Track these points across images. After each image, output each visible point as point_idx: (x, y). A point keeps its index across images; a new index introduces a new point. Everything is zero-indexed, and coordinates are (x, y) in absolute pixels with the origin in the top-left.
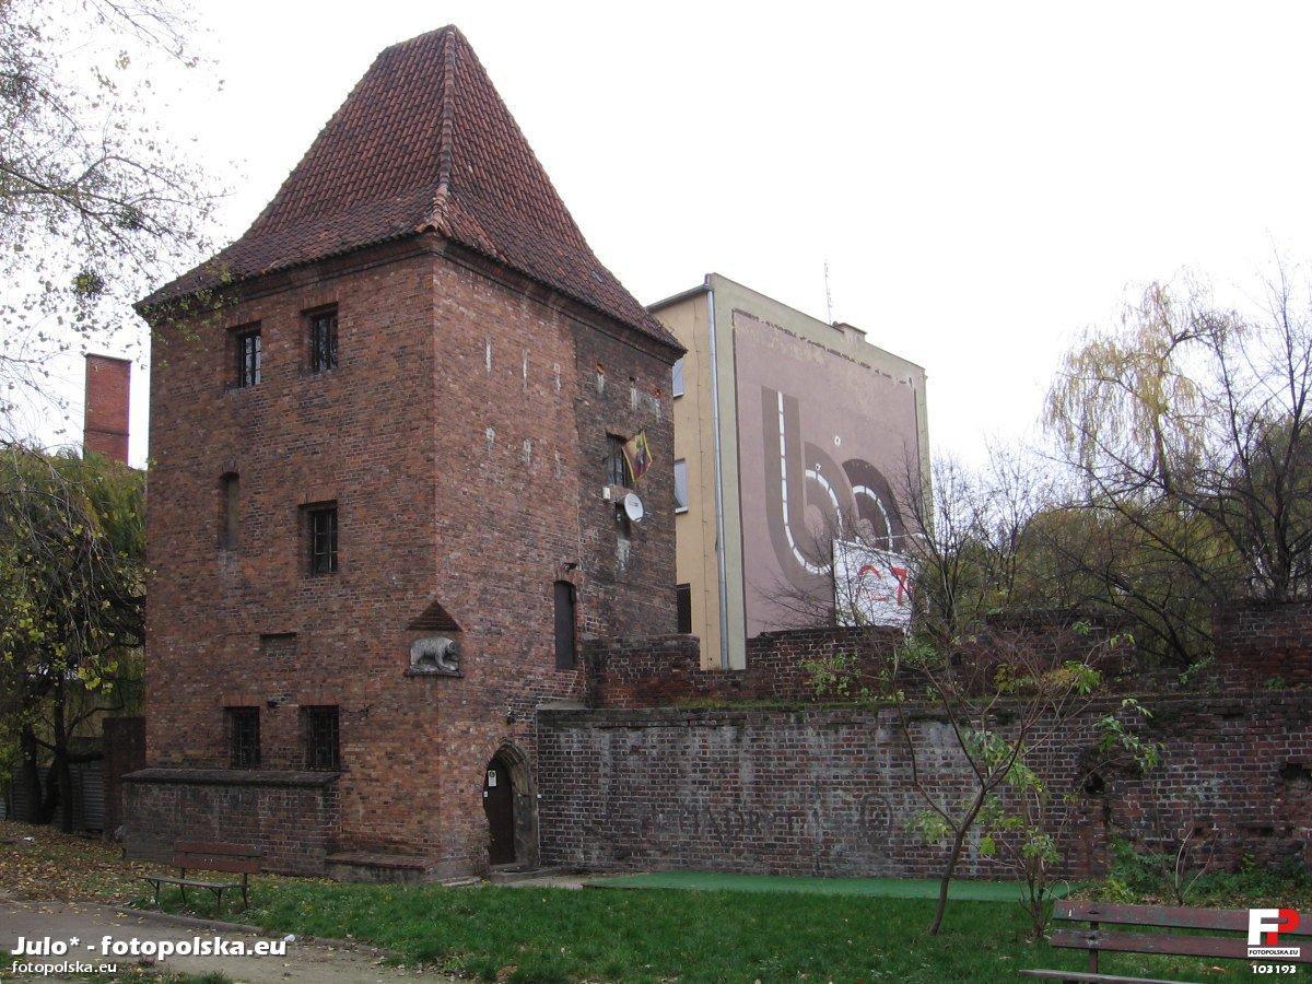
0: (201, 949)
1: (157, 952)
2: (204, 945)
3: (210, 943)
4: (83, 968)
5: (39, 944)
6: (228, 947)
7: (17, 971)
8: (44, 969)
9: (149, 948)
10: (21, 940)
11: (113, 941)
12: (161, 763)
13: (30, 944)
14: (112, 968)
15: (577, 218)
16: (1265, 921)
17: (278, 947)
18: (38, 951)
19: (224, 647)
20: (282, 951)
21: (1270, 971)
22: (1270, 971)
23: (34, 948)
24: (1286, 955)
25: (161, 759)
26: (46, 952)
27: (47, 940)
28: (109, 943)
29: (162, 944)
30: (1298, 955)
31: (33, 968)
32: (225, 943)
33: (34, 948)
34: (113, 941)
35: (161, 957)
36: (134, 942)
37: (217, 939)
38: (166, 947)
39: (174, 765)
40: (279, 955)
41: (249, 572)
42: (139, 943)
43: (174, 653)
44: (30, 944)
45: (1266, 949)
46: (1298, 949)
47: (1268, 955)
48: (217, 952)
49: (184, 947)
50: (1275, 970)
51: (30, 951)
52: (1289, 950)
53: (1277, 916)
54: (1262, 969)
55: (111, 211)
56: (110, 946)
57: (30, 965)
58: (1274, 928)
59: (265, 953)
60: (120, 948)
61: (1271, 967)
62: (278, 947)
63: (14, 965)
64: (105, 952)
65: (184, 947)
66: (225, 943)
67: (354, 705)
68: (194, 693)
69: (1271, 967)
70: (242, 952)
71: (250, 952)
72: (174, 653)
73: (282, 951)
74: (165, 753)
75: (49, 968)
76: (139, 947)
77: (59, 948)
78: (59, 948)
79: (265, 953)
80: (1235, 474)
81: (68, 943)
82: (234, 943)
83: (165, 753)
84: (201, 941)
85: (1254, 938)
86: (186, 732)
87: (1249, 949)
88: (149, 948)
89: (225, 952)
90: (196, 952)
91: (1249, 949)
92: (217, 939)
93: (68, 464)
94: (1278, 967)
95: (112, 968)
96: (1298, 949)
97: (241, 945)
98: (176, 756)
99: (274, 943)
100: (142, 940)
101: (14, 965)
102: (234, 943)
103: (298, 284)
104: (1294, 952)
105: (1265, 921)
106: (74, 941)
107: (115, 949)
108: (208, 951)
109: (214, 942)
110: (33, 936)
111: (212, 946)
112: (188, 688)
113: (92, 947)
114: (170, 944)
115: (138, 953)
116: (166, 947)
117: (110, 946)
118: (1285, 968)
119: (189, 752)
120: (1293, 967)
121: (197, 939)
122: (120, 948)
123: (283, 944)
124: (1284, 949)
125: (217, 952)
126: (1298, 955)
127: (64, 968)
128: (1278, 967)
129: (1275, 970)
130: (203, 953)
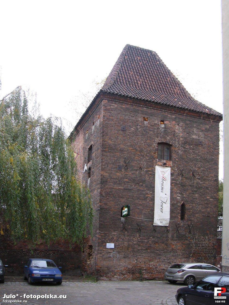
0: (47, 297)
1: (37, 297)
2: (48, 296)
3: (49, 295)
4: (19, 301)
5: (9, 296)
6: (53, 296)
7: (45, 295)
8: (10, 302)
9: (35, 297)
10: (5, 295)
11: (26, 295)
13: (7, 296)
14: (26, 301)
16: (218, 290)
18: (9, 297)
20: (66, 297)
21: (219, 302)
22: (219, 302)
23: (8, 297)
24: (223, 298)
26: (11, 298)
27: (11, 295)
28: (25, 295)
29: (38, 296)
30: (226, 298)
31: (8, 301)
33: (8, 297)
34: (26, 295)
35: (37, 299)
36: (31, 295)
37: (51, 295)
38: (39, 297)
40: (65, 298)
42: (32, 295)
45: (218, 297)
46: (226, 297)
47: (219, 298)
48: (50, 298)
49: (43, 297)
50: (220, 302)
51: (7, 297)
52: (224, 297)
53: (221, 289)
54: (217, 302)
55: (42, 182)
57: (7, 301)
58: (220, 292)
59: (62, 298)
60: (28, 297)
61: (219, 301)
63: (3, 301)
64: (24, 298)
65: (43, 297)
69: (219, 301)
70: (56, 298)
71: (58, 298)
73: (66, 297)
75: (11, 301)
76: (32, 297)
77: (14, 297)
78: (14, 297)
79: (62, 298)
80: (185, 217)
81: (16, 295)
82: (54, 296)
84: (47, 295)
85: (215, 294)
87: (214, 297)
88: (35, 297)
89: (52, 298)
90: (46, 298)
91: (214, 297)
92: (51, 295)
93: (55, 140)
94: (221, 301)
95: (26, 301)
96: (226, 297)
97: (56, 296)
99: (64, 296)
101: (3, 301)
102: (54, 296)
104: (225, 298)
105: (218, 290)
106: (17, 295)
107: (27, 297)
108: (48, 297)
109: (50, 295)
110: (8, 294)
111: (49, 296)
113: (21, 296)
115: (32, 298)
116: (39, 297)
117: (26, 296)
118: (223, 301)
120: (225, 301)
122: (28, 297)
123: (66, 296)
124: (223, 297)
125: (50, 298)
126: (226, 298)
127: (15, 301)
128: (221, 301)
129: (220, 302)
130: (47, 298)
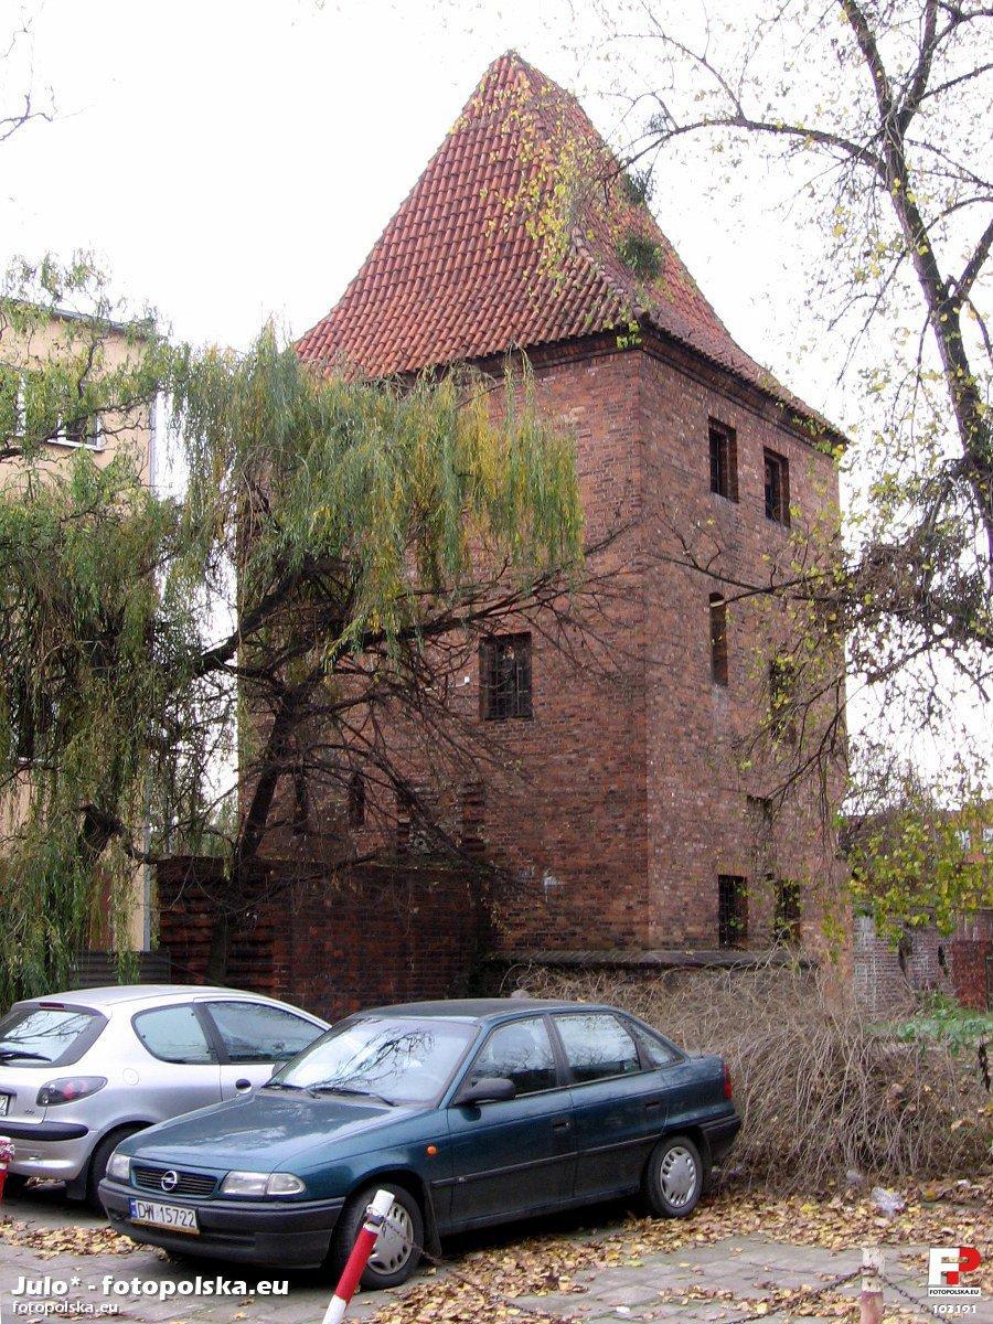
0: (203, 1288)
5: (39, 1283)
6: (230, 1287)
12: (663, 943)
13: (30, 1283)
15: (422, 165)
16: (945, 1260)
17: (280, 1287)
18: (38, 1290)
19: (718, 802)
23: (34, 1286)
25: (662, 938)
26: (47, 1291)
29: (163, 1284)
32: (228, 1283)
33: (34, 1286)
36: (136, 1282)
37: (220, 1279)
38: (167, 1287)
39: (677, 946)
41: (736, 719)
43: (675, 800)
44: (30, 1283)
48: (219, 1292)
49: (185, 1287)
56: (111, 1286)
60: (121, 1287)
62: (280, 1287)
64: (106, 1291)
65: (185, 1287)
66: (228, 1283)
67: (808, 881)
68: (695, 855)
70: (244, 1292)
72: (675, 800)
74: (668, 931)
76: (140, 1287)
83: (668, 931)
84: (203, 1281)
86: (686, 904)
89: (227, 1292)
92: (220, 1279)
97: (243, 1285)
98: (677, 935)
99: (276, 1283)
100: (143, 1280)
103: (765, 415)
112: (690, 847)
114: (172, 1284)
116: (167, 1287)
119: (690, 929)
121: (199, 1279)
122: (121, 1287)
